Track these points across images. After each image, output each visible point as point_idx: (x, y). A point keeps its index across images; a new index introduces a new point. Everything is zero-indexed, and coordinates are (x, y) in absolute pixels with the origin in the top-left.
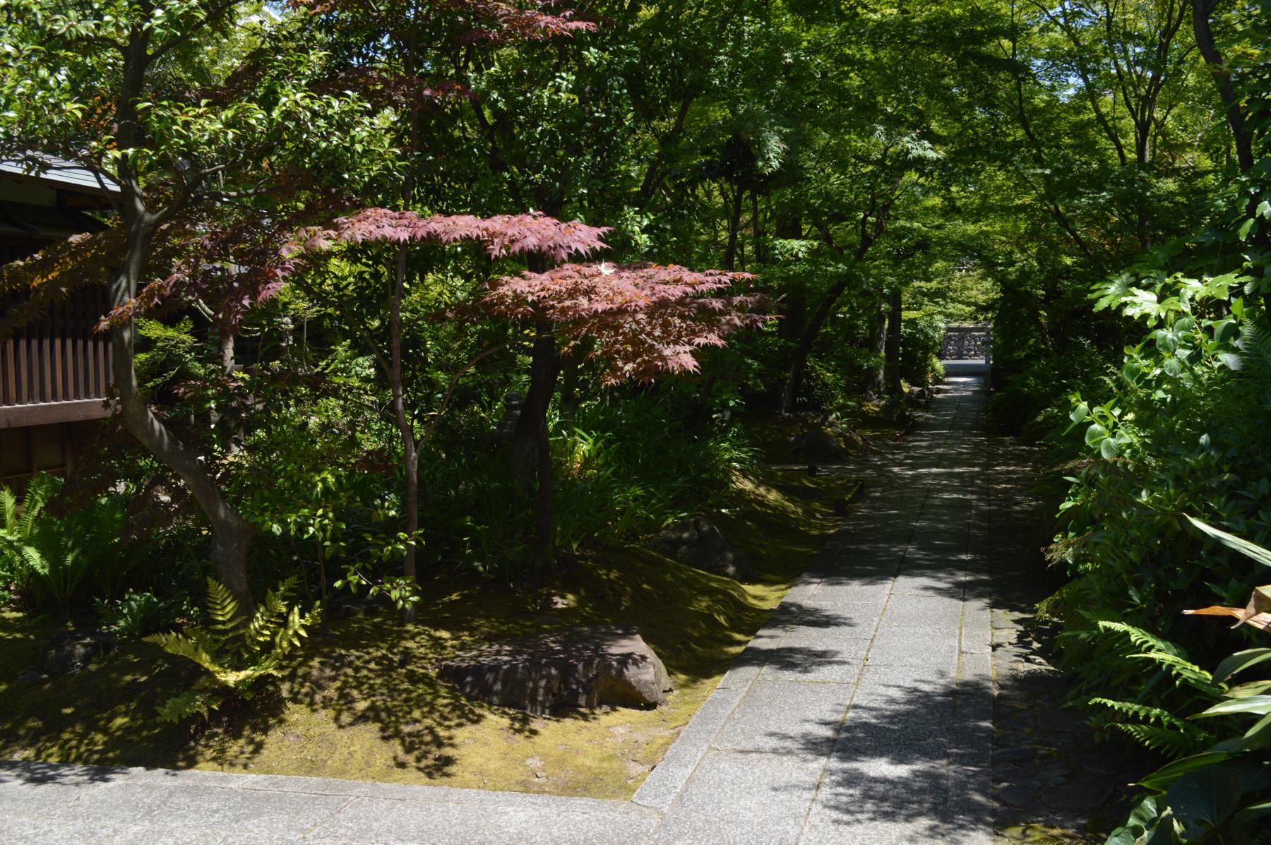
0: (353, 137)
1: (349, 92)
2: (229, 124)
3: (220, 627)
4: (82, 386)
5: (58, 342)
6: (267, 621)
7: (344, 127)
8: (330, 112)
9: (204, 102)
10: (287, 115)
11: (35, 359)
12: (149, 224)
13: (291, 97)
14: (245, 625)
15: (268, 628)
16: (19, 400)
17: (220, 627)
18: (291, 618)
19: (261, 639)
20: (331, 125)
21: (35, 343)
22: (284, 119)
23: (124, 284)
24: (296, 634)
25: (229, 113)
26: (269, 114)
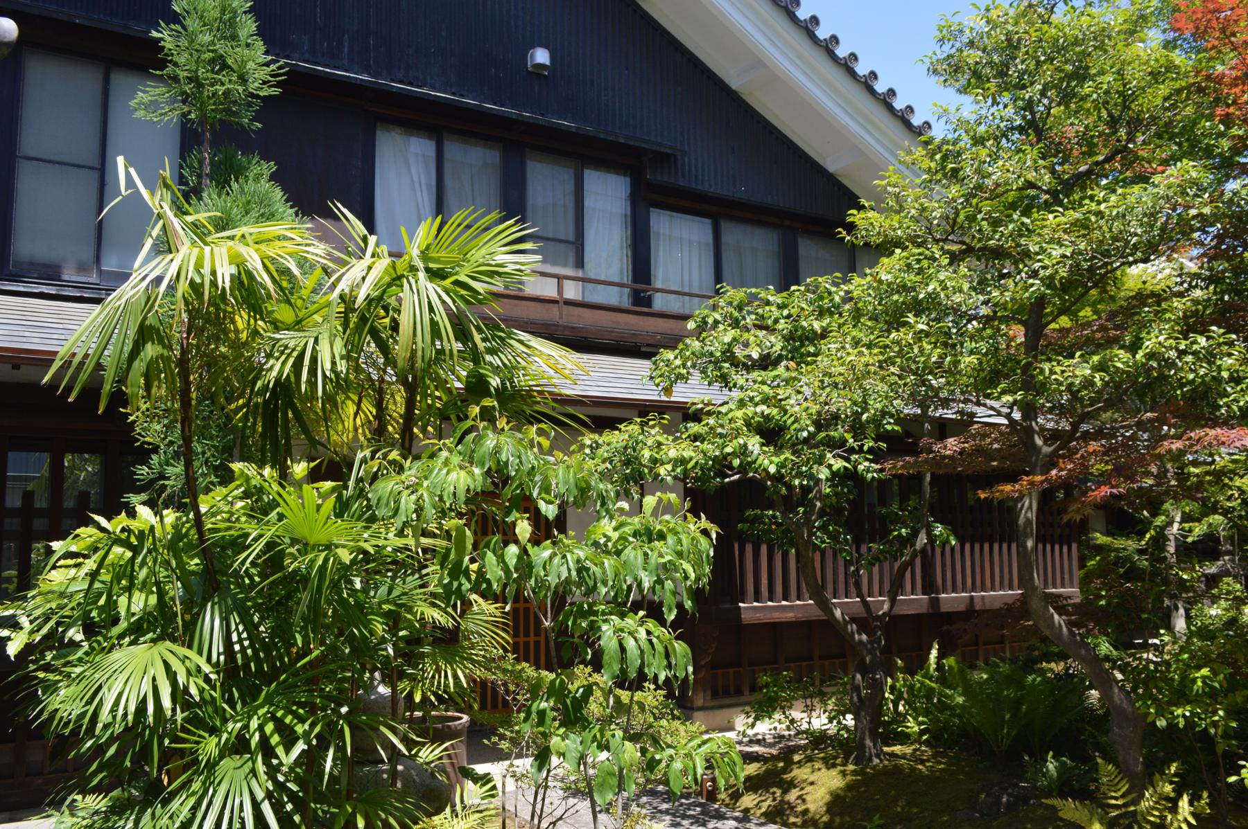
0: (1219, 367)
1: (1214, 328)
2: (1096, 369)
3: (1113, 802)
4: (1067, 576)
5: (986, 546)
6: (1156, 803)
7: (1210, 357)
8: (1195, 347)
9: (1078, 354)
10: (1151, 356)
11: (968, 563)
12: (1046, 456)
13: (1157, 339)
14: (1136, 802)
15: (1157, 809)
16: (993, 589)
17: (1113, 802)
18: (1180, 804)
19: (1152, 819)
20: (1199, 359)
21: (1005, 546)
22: (1148, 360)
23: (1027, 504)
24: (1186, 820)
25: (1096, 358)
26: (1134, 357)
